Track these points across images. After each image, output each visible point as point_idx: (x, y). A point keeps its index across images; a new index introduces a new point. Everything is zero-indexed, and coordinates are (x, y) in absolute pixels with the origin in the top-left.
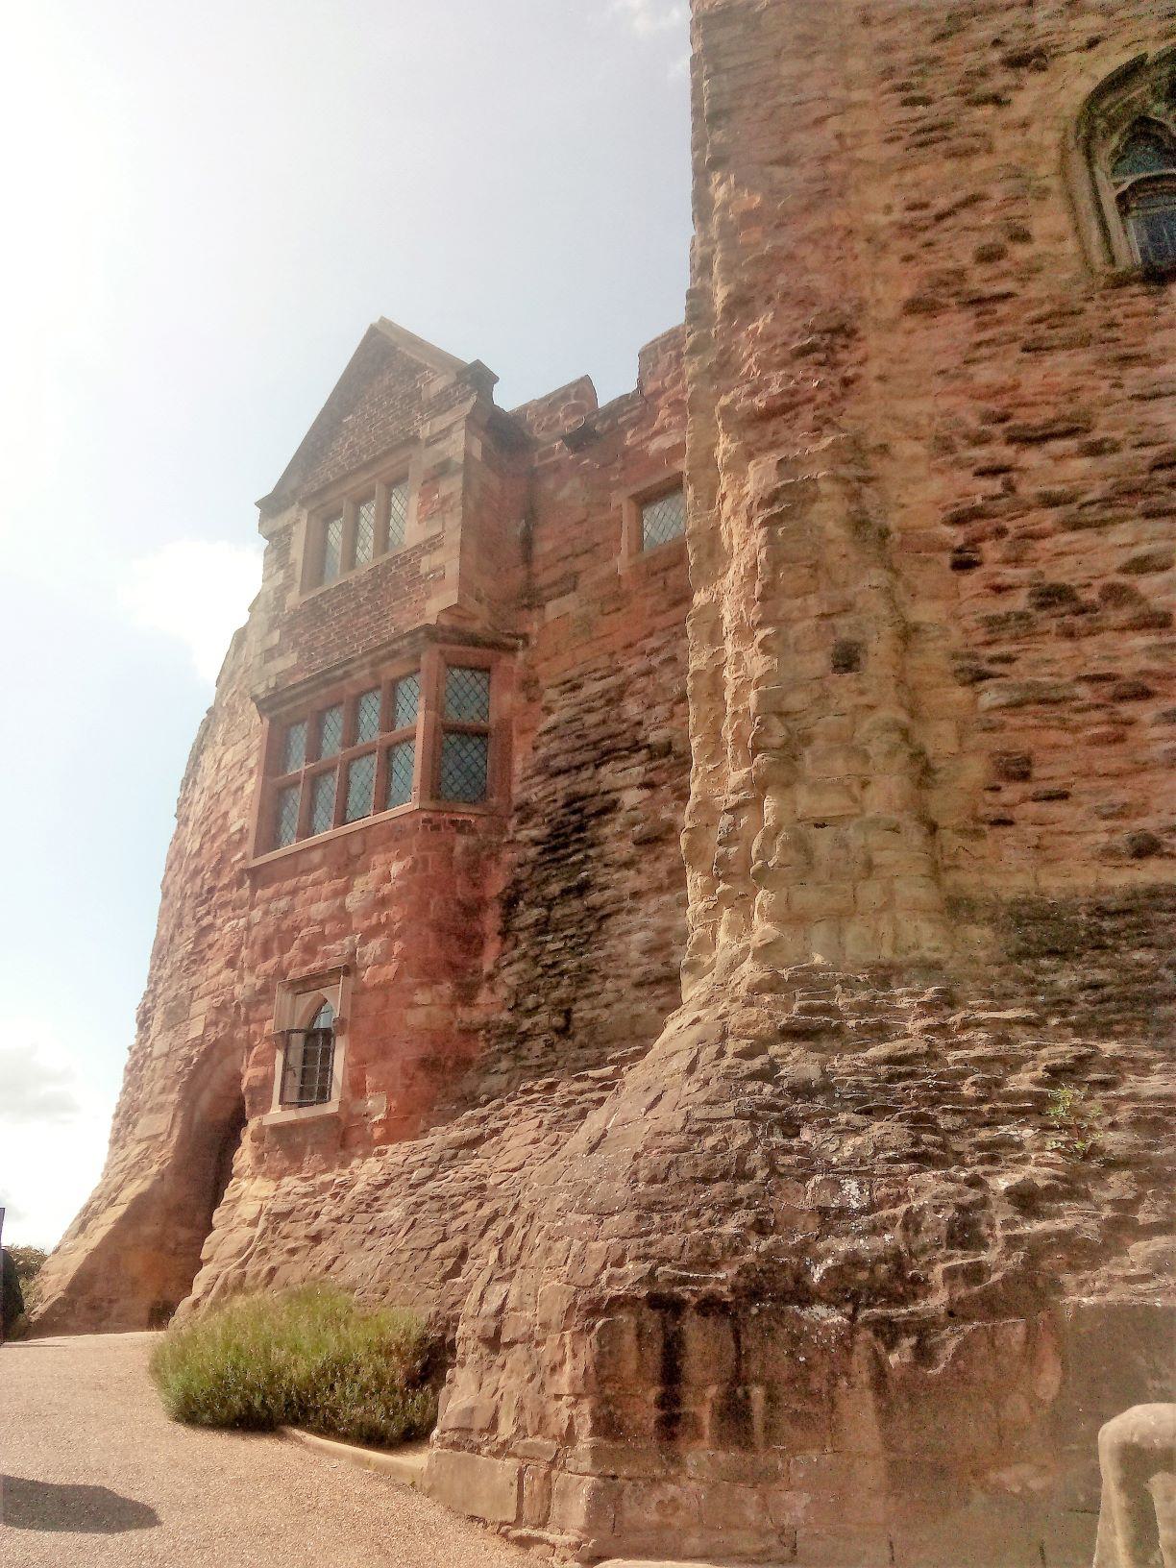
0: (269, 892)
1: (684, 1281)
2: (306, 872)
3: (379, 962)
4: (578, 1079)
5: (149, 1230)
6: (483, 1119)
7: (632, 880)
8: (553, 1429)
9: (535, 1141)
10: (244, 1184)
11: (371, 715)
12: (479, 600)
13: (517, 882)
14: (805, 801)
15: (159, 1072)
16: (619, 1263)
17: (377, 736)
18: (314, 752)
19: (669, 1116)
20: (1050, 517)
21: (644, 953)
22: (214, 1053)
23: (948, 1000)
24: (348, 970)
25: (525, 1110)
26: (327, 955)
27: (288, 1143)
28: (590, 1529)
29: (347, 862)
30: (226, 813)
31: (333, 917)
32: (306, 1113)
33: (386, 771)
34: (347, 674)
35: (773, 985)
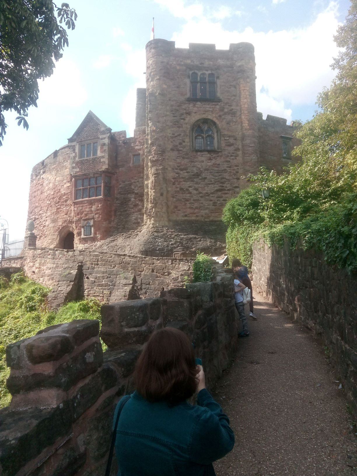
7: (133, 210)
11: (93, 181)
14: (157, 210)
20: (182, 180)
23: (168, 229)
29: (91, 203)
35: (153, 227)
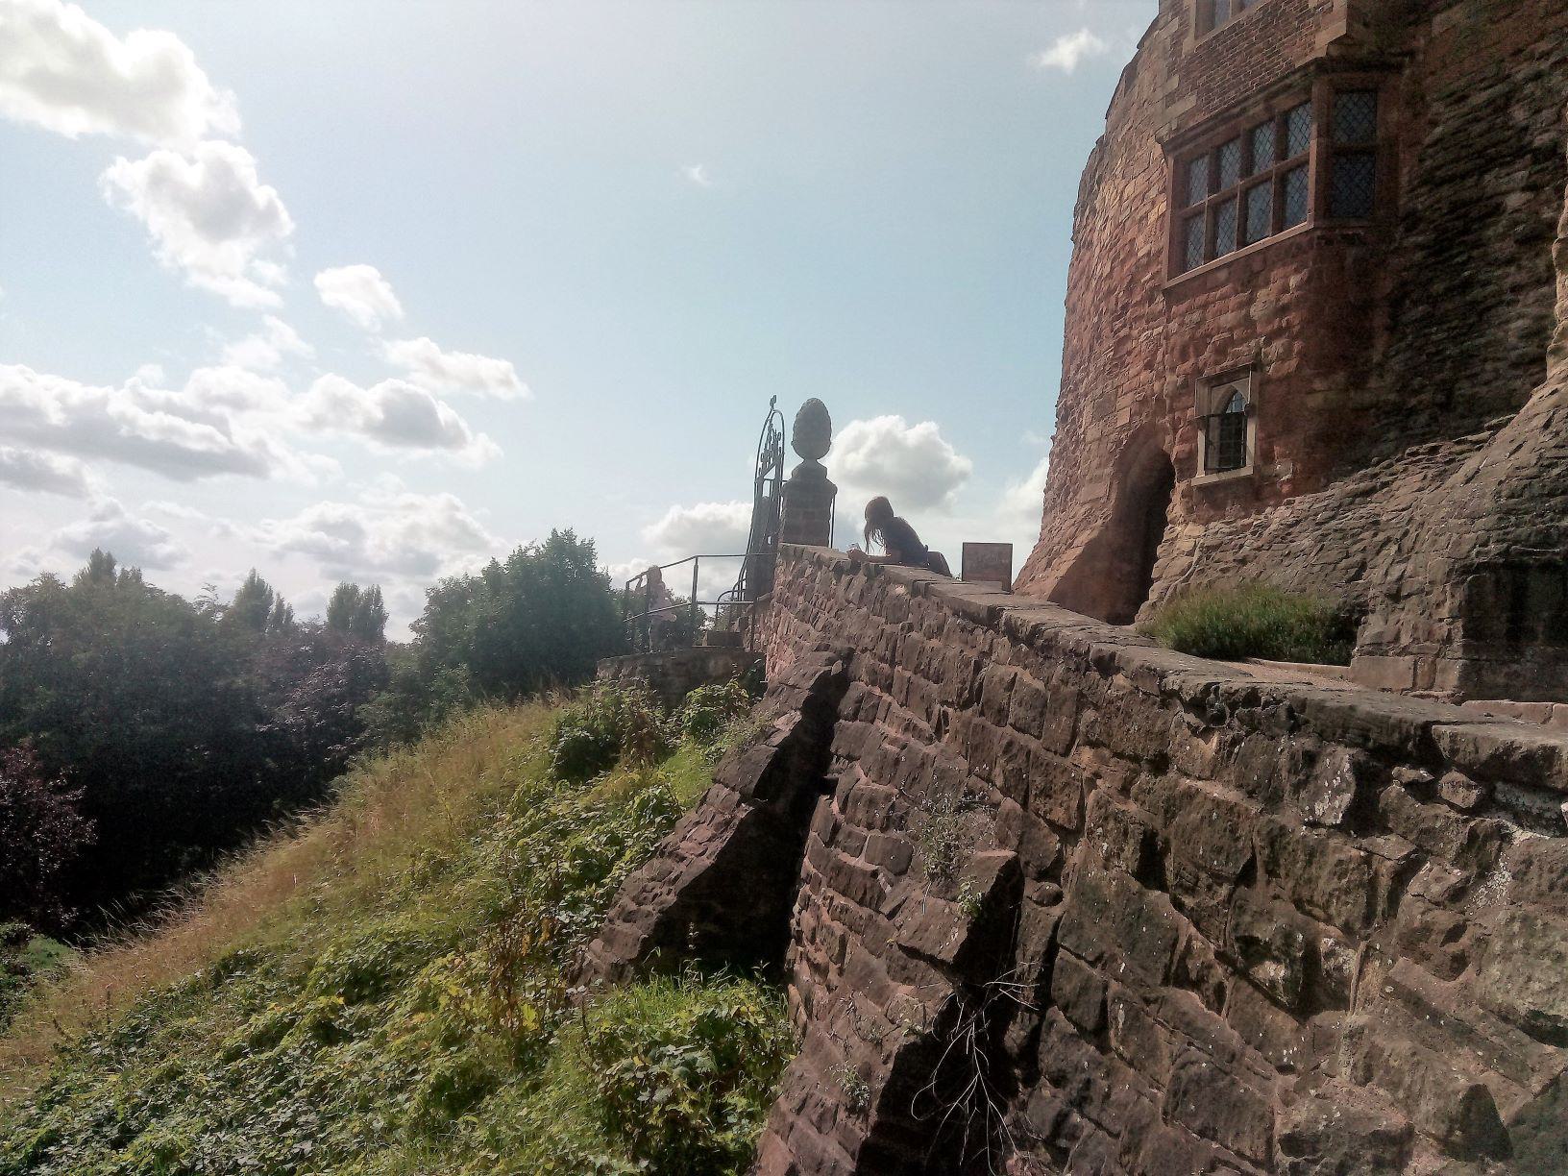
0: (1183, 307)
1: (1530, 553)
2: (1213, 289)
3: (1283, 358)
4: (1458, 443)
5: (1100, 565)
6: (1375, 475)
8: (1437, 636)
9: (1420, 490)
10: (1179, 528)
11: (1266, 143)
12: (1366, 25)
13: (1404, 284)
15: (1094, 453)
16: (1485, 544)
17: (1272, 166)
18: (1215, 184)
19: (1525, 456)
21: (1521, 337)
22: (1142, 435)
24: (1257, 365)
25: (1411, 468)
26: (1237, 355)
27: (1210, 500)
28: (1460, 687)
29: (1249, 276)
30: (1133, 241)
31: (1239, 325)
32: (1225, 476)
33: (1281, 194)
34: (1244, 110)
